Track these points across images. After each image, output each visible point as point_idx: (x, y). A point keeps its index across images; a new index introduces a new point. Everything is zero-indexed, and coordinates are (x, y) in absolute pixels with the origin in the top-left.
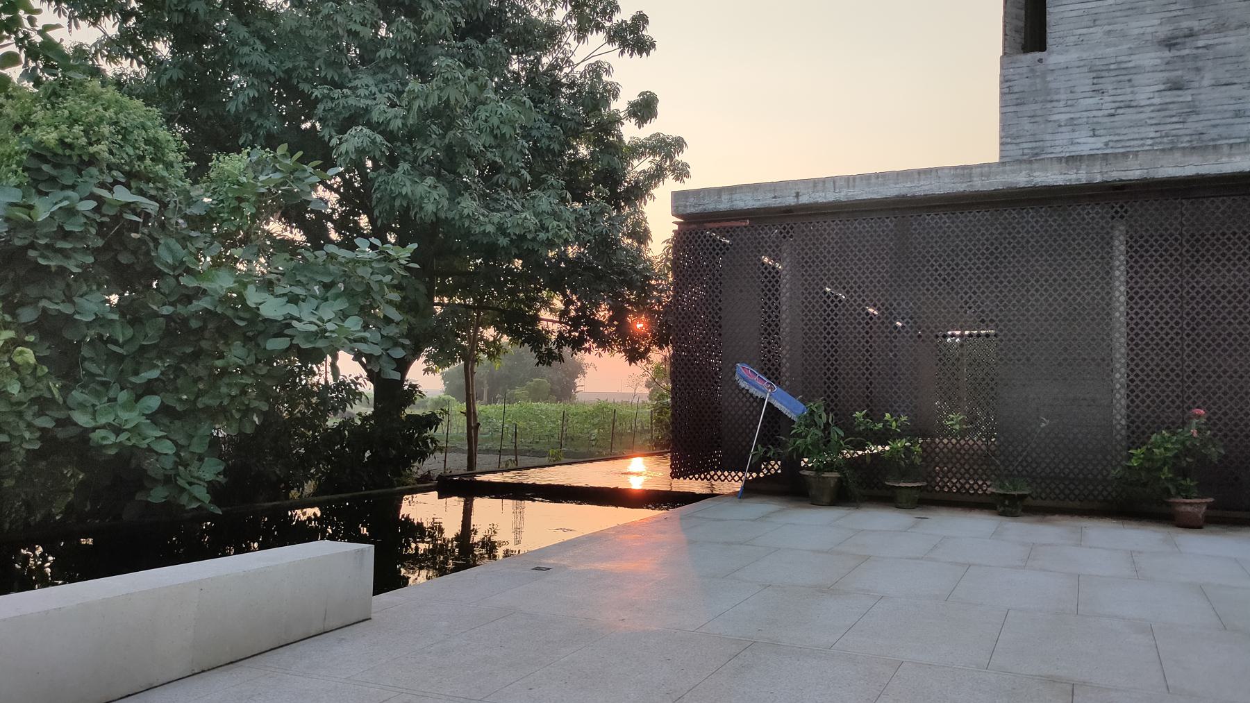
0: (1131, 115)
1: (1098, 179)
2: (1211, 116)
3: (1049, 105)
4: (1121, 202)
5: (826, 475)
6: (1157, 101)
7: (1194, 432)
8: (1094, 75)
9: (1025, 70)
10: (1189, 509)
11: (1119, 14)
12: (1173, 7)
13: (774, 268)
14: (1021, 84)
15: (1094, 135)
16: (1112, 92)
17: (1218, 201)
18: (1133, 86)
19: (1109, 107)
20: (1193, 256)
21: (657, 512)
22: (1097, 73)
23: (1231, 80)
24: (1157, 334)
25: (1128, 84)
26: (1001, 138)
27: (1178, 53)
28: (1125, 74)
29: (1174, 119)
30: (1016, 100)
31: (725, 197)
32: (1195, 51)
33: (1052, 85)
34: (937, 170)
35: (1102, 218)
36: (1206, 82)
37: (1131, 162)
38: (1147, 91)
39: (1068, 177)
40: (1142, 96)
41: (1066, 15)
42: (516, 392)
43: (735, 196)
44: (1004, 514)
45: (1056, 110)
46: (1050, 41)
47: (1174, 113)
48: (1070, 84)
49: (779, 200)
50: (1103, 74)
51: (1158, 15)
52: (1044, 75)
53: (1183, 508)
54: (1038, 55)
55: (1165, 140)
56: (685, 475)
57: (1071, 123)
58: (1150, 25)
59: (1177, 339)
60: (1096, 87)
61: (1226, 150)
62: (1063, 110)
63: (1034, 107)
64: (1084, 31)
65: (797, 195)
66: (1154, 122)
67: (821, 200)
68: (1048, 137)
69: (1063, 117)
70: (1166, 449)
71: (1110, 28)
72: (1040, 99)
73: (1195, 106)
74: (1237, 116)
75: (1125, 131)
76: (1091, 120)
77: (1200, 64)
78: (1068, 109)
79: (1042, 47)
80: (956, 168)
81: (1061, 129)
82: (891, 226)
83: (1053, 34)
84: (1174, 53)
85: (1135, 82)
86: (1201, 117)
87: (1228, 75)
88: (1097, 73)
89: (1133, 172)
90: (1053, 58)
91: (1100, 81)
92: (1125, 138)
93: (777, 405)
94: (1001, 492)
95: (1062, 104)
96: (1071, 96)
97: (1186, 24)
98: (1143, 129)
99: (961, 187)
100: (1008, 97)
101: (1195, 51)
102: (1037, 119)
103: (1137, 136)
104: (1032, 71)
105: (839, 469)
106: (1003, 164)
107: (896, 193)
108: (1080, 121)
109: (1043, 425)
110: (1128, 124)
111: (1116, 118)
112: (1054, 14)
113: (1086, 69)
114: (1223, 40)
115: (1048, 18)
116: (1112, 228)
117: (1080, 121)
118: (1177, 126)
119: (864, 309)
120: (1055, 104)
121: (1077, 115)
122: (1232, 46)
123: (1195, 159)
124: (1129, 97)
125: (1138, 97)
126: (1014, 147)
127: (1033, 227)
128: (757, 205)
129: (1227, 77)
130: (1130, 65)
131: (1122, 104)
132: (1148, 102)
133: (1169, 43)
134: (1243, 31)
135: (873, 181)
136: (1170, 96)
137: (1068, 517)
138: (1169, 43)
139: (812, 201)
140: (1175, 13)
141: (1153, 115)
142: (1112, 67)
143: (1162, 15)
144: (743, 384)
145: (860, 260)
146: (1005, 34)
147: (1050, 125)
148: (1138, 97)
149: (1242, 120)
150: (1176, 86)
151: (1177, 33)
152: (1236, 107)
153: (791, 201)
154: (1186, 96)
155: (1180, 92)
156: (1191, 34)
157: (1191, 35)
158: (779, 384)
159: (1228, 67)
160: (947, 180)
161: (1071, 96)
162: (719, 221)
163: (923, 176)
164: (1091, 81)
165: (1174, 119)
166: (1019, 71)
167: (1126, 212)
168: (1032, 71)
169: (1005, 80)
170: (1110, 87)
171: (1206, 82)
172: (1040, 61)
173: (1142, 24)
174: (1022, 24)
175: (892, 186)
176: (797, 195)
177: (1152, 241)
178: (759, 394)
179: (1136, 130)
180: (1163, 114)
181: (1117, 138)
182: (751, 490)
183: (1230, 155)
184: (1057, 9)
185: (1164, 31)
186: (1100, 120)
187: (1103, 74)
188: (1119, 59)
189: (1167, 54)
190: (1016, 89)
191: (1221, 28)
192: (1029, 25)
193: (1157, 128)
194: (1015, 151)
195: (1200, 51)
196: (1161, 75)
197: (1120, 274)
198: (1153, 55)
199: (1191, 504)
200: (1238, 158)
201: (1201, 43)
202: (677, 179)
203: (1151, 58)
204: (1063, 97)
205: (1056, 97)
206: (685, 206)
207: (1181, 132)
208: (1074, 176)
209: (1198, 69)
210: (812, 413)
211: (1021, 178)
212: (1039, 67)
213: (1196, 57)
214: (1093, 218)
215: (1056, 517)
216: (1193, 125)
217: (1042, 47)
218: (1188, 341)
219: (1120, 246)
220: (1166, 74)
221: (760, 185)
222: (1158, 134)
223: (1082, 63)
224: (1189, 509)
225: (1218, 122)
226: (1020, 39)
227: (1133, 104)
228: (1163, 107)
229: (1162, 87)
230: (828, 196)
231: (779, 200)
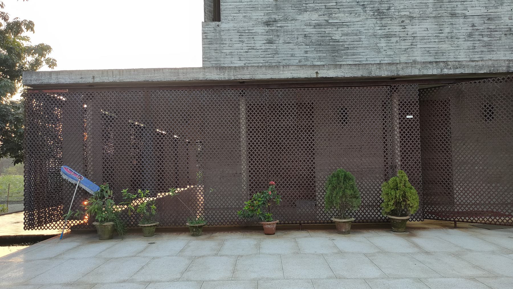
0: (253, 53)
1: (233, 78)
2: (283, 55)
3: (222, 46)
4: (242, 89)
5: (106, 224)
6: (263, 47)
7: (270, 192)
8: (240, 34)
9: (212, 29)
10: (269, 226)
11: (248, 9)
12: (269, 9)
13: (105, 115)
14: (211, 35)
15: (240, 60)
16: (246, 42)
17: (279, 90)
18: (254, 40)
19: (245, 48)
20: (270, 114)
21: (25, 247)
22: (241, 33)
23: (290, 41)
24: (257, 148)
25: (252, 39)
26: (203, 58)
27: (271, 28)
28: (252, 35)
29: (270, 56)
30: (208, 42)
31: (54, 76)
32: (277, 28)
33: (223, 37)
34: (163, 69)
35: (235, 96)
36: (281, 41)
37: (245, 71)
38: (260, 42)
39: (220, 76)
40: (258, 45)
41: (228, 7)
42: (9, 169)
43: (59, 76)
44: (193, 235)
45: (225, 48)
46: (222, 17)
47: (269, 53)
48: (230, 37)
49: (84, 80)
50: (243, 34)
51: (263, 12)
52: (220, 32)
53: (267, 226)
54: (217, 23)
55: (267, 64)
56: (40, 224)
57: (231, 54)
58: (260, 15)
59: (265, 150)
60: (240, 40)
61: (282, 68)
62: (228, 48)
63: (216, 46)
64: (235, 15)
65: (94, 78)
66: (262, 56)
67: (106, 81)
68: (222, 59)
69: (228, 51)
70: (259, 201)
71: (245, 14)
72: (218, 42)
73: (277, 51)
74: (292, 56)
75: (251, 59)
76: (239, 53)
77: (279, 34)
78: (229, 48)
79: (219, 20)
80: (171, 69)
81: (227, 57)
82: (142, 95)
83: (223, 14)
84: (269, 28)
85: (255, 39)
86: (280, 56)
87: (289, 39)
88: (241, 33)
89: (246, 75)
90: (224, 25)
91: (242, 37)
92: (252, 62)
93: (84, 187)
94: (192, 225)
95: (227, 45)
96: (231, 42)
97: (273, 16)
98: (258, 59)
99: (174, 78)
100: (206, 40)
101: (277, 28)
102: (218, 51)
103: (256, 62)
104: (215, 30)
105: (112, 220)
106: (204, 68)
107: (144, 79)
108: (234, 53)
109: (211, 191)
110: (253, 56)
111: (248, 53)
112: (223, 6)
113: (236, 31)
114: (286, 25)
115: (221, 7)
116: (239, 100)
117: (234, 53)
118: (271, 59)
119: (167, 132)
120: (224, 45)
121: (233, 51)
122: (290, 28)
123: (270, 71)
124: (253, 45)
125: (257, 45)
126: (209, 63)
127: (206, 99)
128: (72, 82)
129: (288, 40)
130: (253, 31)
131: (250, 48)
132: (260, 48)
133: (267, 24)
134: (293, 22)
135: (132, 72)
136: (268, 46)
137: (222, 233)
138: (267, 24)
139: (101, 81)
140: (269, 11)
141: (262, 53)
142: (246, 31)
143: (265, 11)
144: (65, 177)
145: (126, 112)
146: (205, 13)
147: (223, 54)
148: (257, 45)
149: (293, 58)
150: (270, 42)
151: (270, 20)
152: (291, 53)
153: (90, 80)
154: (274, 46)
155: (272, 45)
156: (275, 21)
157: (275, 21)
158: (86, 176)
159: (289, 36)
160: (168, 75)
161: (231, 42)
162: (52, 89)
163: (156, 72)
164: (238, 37)
165: (270, 56)
166: (209, 29)
167: (244, 93)
168: (215, 30)
169: (204, 33)
170: (246, 40)
171: (281, 41)
172: (218, 26)
173: (257, 14)
174: (212, 9)
175: (142, 76)
176: (94, 78)
177: (254, 107)
178: (74, 182)
179: (256, 59)
180: (266, 53)
181: (249, 62)
182: (76, 231)
183: (283, 71)
184: (224, 4)
185: (266, 18)
186: (242, 54)
187: (243, 34)
188: (249, 28)
189: (267, 28)
190: (209, 37)
191: (286, 20)
192: (214, 11)
193: (264, 59)
194: (208, 64)
195: (279, 28)
196: (265, 37)
197: (243, 121)
198: (261, 28)
199: (270, 224)
200: (286, 72)
201: (279, 25)
202: (50, 67)
203: (261, 29)
204: (227, 42)
205: (225, 42)
206: (31, 80)
207: (273, 61)
208: (223, 76)
209: (278, 36)
210: (102, 191)
211: (214, 76)
212: (218, 28)
213: (277, 30)
214: (231, 96)
215: (217, 234)
216: (276, 59)
217: (219, 20)
218: (269, 151)
219: (243, 108)
220: (266, 37)
221: (73, 71)
222: (264, 62)
223: (235, 29)
224: (269, 226)
225: (285, 58)
226: (211, 15)
227: (255, 48)
228: (266, 50)
229: (265, 42)
230: (107, 79)
231: (84, 80)
